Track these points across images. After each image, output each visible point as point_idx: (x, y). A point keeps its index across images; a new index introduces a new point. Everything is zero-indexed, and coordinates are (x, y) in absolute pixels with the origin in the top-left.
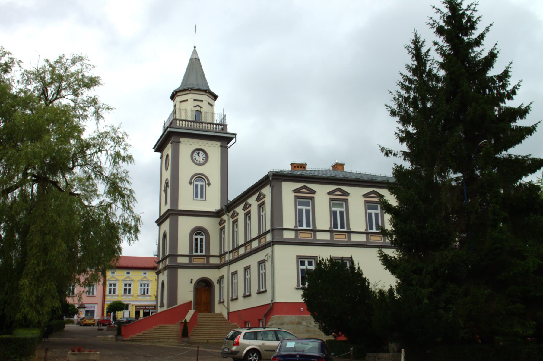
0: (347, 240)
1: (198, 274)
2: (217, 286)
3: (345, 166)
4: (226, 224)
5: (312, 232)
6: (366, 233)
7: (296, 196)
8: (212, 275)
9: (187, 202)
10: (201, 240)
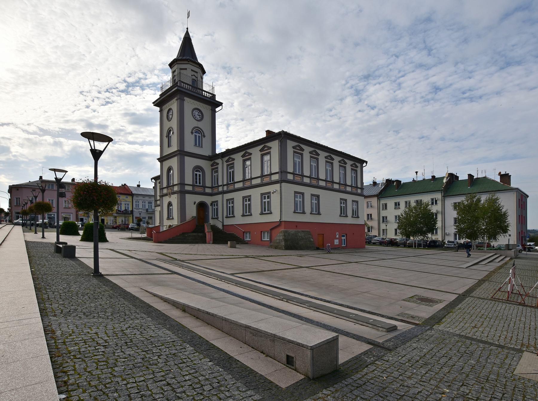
1: (199, 199)
2: (210, 207)
4: (220, 167)
6: (310, 177)
8: (208, 200)
9: (190, 147)
10: (200, 175)
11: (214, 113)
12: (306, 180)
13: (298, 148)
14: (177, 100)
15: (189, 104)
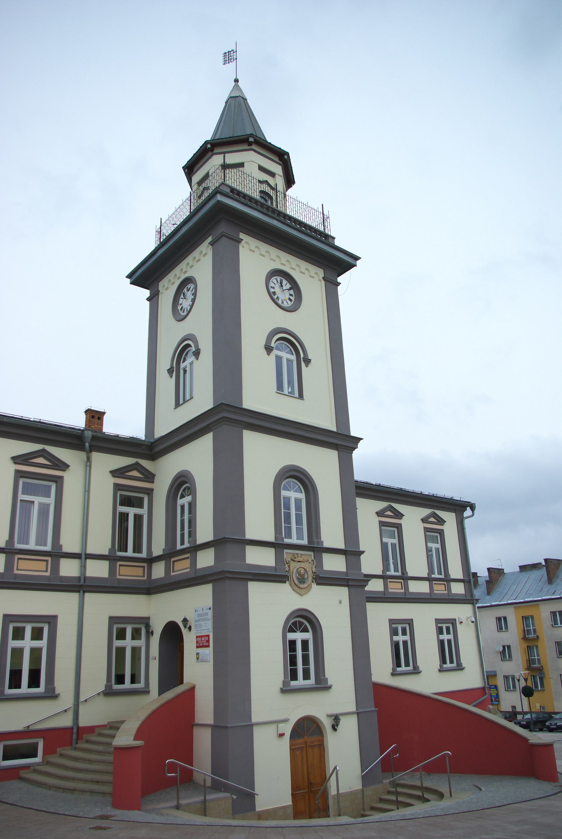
0: (48, 574)
3: (105, 417)
5: (49, 559)
6: (428, 579)
7: (17, 472)
11: (332, 285)
12: (415, 587)
13: (389, 513)
14: (212, 244)
15: (256, 260)
